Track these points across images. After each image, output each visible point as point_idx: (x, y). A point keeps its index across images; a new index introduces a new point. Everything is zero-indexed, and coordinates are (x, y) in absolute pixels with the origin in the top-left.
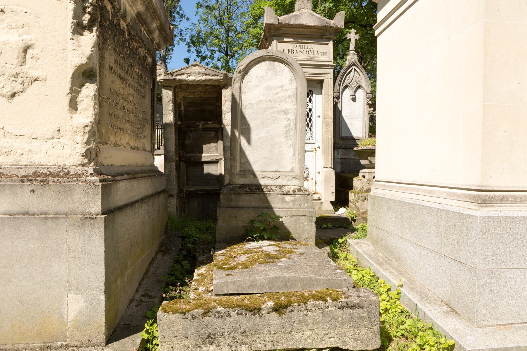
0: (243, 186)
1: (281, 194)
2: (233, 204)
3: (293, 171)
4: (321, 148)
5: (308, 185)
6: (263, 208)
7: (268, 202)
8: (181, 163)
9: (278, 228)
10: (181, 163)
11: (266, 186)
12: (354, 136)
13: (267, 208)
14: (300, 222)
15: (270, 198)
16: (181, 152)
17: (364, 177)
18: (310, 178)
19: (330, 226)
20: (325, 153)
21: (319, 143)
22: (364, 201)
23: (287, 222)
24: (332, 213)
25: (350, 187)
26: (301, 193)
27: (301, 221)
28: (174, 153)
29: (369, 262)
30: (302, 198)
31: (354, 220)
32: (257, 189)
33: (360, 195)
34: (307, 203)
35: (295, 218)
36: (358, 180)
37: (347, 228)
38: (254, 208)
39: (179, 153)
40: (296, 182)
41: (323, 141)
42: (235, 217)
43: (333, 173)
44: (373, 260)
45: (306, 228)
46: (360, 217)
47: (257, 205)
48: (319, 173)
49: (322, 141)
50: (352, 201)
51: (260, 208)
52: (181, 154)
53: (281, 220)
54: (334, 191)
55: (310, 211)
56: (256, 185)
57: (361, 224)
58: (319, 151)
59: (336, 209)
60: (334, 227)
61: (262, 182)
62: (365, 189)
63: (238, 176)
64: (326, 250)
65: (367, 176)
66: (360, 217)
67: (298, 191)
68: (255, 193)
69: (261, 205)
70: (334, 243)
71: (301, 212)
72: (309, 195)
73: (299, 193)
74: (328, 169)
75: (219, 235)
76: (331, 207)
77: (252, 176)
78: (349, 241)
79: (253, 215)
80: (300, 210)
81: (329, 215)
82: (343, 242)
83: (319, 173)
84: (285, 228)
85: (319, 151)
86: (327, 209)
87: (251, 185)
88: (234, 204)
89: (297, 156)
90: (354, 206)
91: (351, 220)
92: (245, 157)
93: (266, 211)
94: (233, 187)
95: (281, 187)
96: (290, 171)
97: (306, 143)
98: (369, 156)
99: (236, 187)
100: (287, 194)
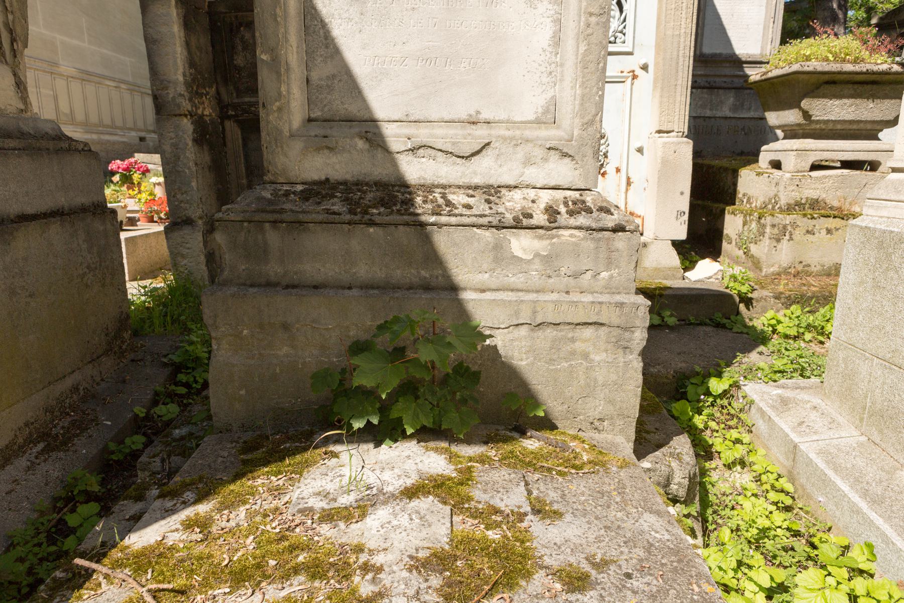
0: (318, 191)
1: (490, 226)
2: (274, 269)
3: (549, 116)
4: (651, 68)
5: (609, 188)
6: (410, 288)
7: (434, 259)
8: (228, 124)
9: (475, 377)
10: (228, 124)
11: (429, 188)
12: (737, 52)
13: (427, 287)
14: (573, 353)
15: (442, 241)
16: (223, 90)
17: (777, 165)
18: (610, 169)
19: (672, 321)
20: (663, 84)
21: (646, 54)
22: (778, 240)
23: (513, 345)
24: (674, 277)
25: (729, 196)
26: (582, 220)
27: (579, 346)
28: (181, 89)
29: (871, 523)
30: (590, 245)
31: (748, 302)
32: (387, 201)
33: (768, 220)
34: (609, 264)
35: (550, 332)
36: (758, 174)
37: (723, 326)
38: (367, 287)
39: (218, 93)
40: (562, 172)
41: (660, 46)
42: (286, 327)
43: (687, 149)
44: (888, 519)
45: (600, 376)
46: (765, 293)
47: (379, 273)
48: (640, 150)
49: (658, 46)
50: (734, 237)
51: (396, 287)
52: (225, 98)
53: (488, 342)
54: (686, 208)
55: (621, 305)
56: (379, 185)
57: (770, 314)
58: (646, 80)
59: (688, 264)
60: (685, 323)
61: (414, 170)
62: (783, 202)
63: (297, 146)
64: (678, 457)
65: (790, 162)
66: (765, 293)
67: (571, 213)
68: (371, 223)
69: (400, 273)
70: (690, 390)
71: (583, 304)
72: (619, 229)
73: (572, 222)
74: (672, 138)
75: (226, 396)
76: (673, 259)
77: (360, 144)
78: (751, 389)
79: (360, 318)
80: (575, 297)
81: (668, 283)
82: (725, 392)
83: (640, 150)
84: (512, 374)
85: (646, 80)
86: (661, 262)
87: (358, 183)
88: (280, 270)
89: (569, 44)
90: (741, 253)
91: (737, 299)
92: (332, 51)
93: (416, 308)
94: (275, 193)
95: (491, 192)
96: (538, 122)
97: (611, 54)
98: (805, 96)
99: (287, 194)
100: (517, 225)
